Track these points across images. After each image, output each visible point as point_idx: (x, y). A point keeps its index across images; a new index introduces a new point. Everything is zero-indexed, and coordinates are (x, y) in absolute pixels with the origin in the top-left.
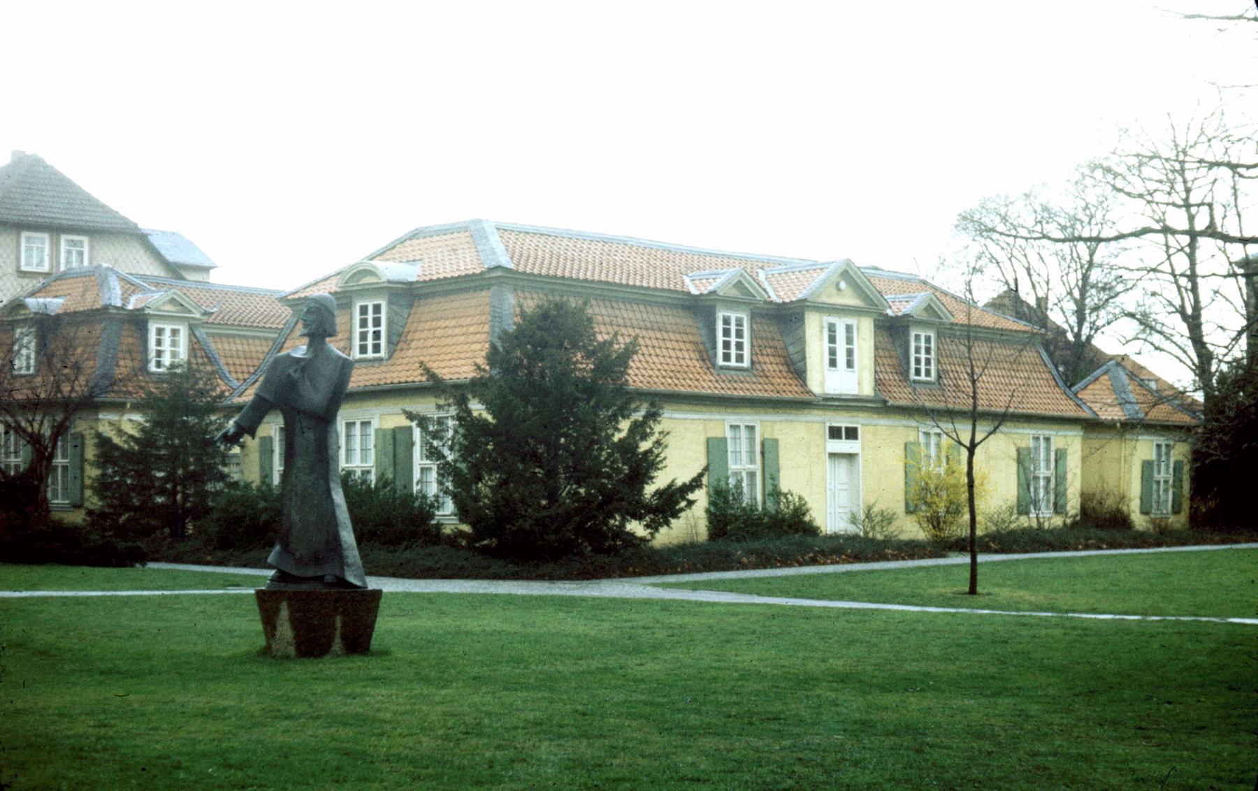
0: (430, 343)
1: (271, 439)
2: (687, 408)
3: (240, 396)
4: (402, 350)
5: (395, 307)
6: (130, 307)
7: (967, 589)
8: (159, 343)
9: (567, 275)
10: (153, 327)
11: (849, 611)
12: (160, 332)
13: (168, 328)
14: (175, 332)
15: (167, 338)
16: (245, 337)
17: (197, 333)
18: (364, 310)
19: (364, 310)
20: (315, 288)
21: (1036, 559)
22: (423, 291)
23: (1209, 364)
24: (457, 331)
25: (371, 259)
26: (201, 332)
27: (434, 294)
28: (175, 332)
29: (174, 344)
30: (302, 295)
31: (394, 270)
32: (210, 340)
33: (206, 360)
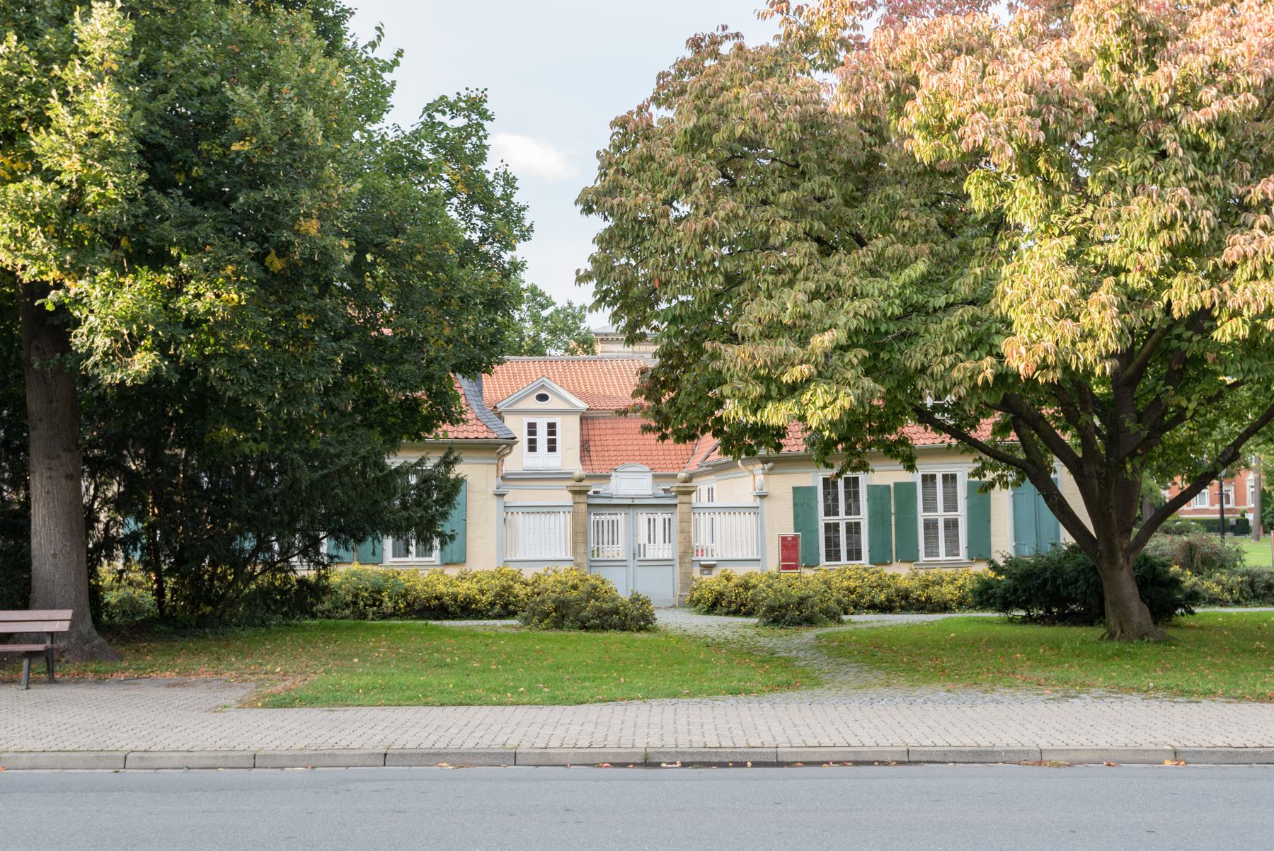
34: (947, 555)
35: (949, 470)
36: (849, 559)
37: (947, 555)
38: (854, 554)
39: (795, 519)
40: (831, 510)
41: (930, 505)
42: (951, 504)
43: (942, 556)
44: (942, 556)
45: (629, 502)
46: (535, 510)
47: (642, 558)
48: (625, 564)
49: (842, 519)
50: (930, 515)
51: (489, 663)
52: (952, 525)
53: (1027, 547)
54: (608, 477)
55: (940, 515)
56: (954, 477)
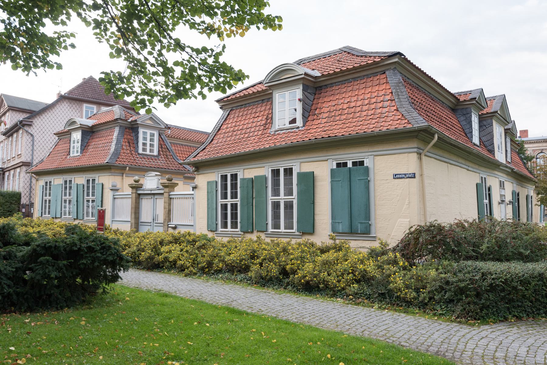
3: (195, 157)
5: (306, 93)
10: (141, 131)
12: (145, 133)
34: (285, 229)
35: (288, 165)
36: (232, 228)
37: (285, 229)
38: (234, 225)
39: (208, 201)
40: (276, 192)
41: (276, 192)
42: (289, 192)
43: (282, 229)
44: (282, 229)
45: (149, 192)
46: (186, 196)
47: (157, 222)
48: (149, 224)
49: (229, 201)
50: (234, 201)
51: (446, 253)
52: (289, 206)
53: (341, 225)
54: (194, 178)
55: (282, 198)
56: (291, 170)
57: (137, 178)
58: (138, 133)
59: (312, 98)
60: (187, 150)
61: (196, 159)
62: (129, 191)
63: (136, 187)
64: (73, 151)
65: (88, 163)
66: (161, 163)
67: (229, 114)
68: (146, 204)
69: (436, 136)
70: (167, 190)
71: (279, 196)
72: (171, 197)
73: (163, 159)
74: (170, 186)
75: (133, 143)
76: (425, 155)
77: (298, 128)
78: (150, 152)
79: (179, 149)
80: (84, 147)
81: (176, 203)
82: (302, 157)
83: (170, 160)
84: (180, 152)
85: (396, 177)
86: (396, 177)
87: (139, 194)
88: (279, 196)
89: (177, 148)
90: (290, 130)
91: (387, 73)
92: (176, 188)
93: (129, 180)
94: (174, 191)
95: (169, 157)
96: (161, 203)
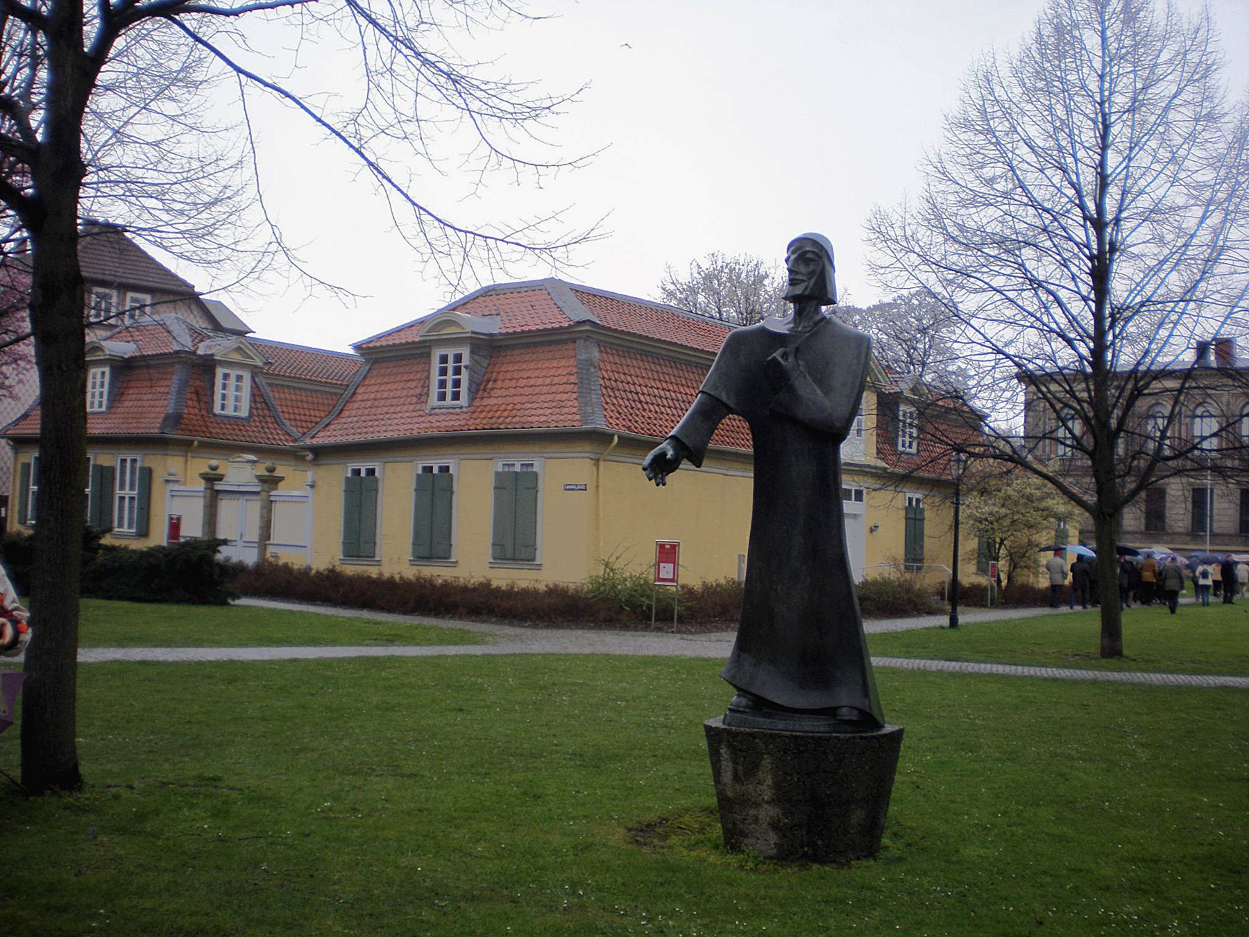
0: (512, 391)
1: (29, 465)
2: (740, 466)
3: (312, 438)
4: (482, 398)
5: (476, 357)
6: (200, 352)
7: (1096, 641)
8: (224, 387)
9: (88, 425)
10: (220, 372)
11: (1178, 690)
12: (226, 376)
13: (233, 373)
14: (239, 378)
15: (232, 382)
16: (294, 388)
17: (257, 380)
18: (444, 359)
19: (444, 359)
20: (409, 332)
21: (29, 475)
22: (502, 343)
23: (1112, 446)
24: (540, 381)
25: (454, 309)
26: (260, 380)
27: (513, 347)
28: (239, 378)
29: (238, 388)
30: (378, 344)
31: (474, 323)
32: (268, 389)
33: (264, 406)
45: (236, 489)
57: (214, 463)
58: (214, 375)
59: (485, 363)
60: (304, 399)
61: (315, 441)
62: (201, 485)
63: (211, 478)
64: (92, 404)
65: (125, 431)
66: (253, 431)
67: (370, 369)
68: (226, 507)
69: (616, 439)
70: (266, 486)
71: (113, 469)
72: (272, 498)
73: (258, 424)
74: (271, 481)
75: (204, 395)
76: (605, 460)
77: (461, 408)
78: (235, 411)
79: (288, 396)
80: (116, 396)
81: (278, 511)
82: (462, 452)
83: (271, 426)
84: (289, 403)
85: (569, 488)
86: (569, 488)
87: (218, 492)
88: (113, 469)
89: (282, 396)
90: (450, 410)
91: (578, 342)
92: (281, 484)
93: (202, 464)
94: (276, 489)
95: (268, 419)
96: (254, 509)
